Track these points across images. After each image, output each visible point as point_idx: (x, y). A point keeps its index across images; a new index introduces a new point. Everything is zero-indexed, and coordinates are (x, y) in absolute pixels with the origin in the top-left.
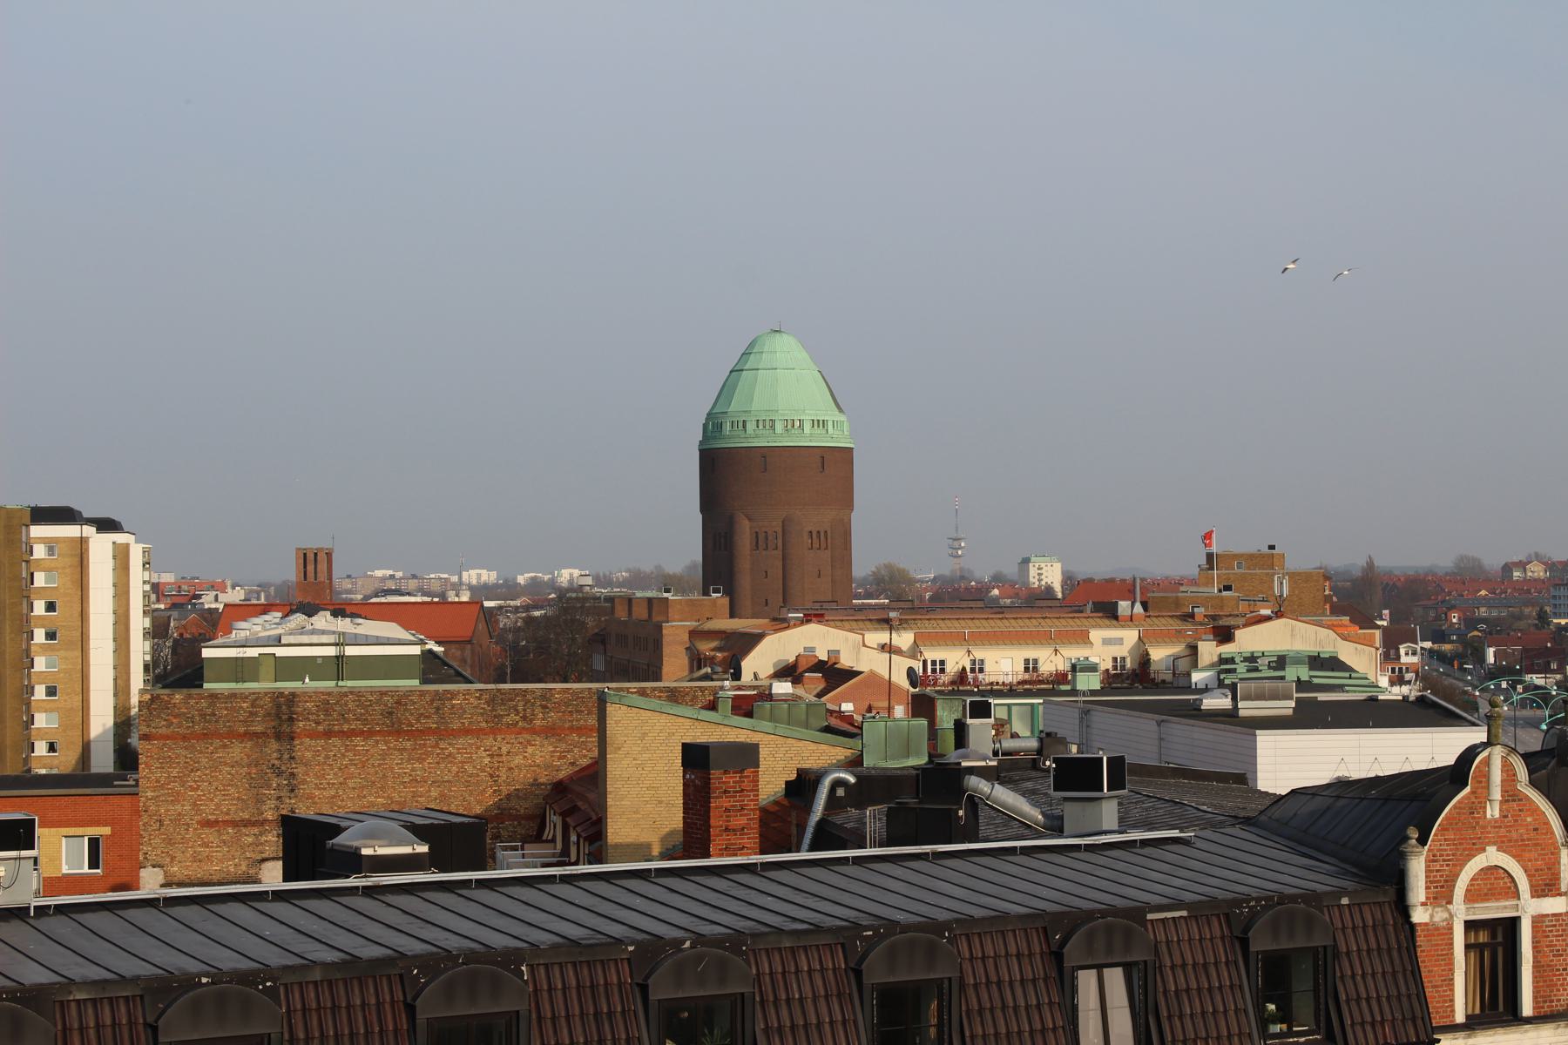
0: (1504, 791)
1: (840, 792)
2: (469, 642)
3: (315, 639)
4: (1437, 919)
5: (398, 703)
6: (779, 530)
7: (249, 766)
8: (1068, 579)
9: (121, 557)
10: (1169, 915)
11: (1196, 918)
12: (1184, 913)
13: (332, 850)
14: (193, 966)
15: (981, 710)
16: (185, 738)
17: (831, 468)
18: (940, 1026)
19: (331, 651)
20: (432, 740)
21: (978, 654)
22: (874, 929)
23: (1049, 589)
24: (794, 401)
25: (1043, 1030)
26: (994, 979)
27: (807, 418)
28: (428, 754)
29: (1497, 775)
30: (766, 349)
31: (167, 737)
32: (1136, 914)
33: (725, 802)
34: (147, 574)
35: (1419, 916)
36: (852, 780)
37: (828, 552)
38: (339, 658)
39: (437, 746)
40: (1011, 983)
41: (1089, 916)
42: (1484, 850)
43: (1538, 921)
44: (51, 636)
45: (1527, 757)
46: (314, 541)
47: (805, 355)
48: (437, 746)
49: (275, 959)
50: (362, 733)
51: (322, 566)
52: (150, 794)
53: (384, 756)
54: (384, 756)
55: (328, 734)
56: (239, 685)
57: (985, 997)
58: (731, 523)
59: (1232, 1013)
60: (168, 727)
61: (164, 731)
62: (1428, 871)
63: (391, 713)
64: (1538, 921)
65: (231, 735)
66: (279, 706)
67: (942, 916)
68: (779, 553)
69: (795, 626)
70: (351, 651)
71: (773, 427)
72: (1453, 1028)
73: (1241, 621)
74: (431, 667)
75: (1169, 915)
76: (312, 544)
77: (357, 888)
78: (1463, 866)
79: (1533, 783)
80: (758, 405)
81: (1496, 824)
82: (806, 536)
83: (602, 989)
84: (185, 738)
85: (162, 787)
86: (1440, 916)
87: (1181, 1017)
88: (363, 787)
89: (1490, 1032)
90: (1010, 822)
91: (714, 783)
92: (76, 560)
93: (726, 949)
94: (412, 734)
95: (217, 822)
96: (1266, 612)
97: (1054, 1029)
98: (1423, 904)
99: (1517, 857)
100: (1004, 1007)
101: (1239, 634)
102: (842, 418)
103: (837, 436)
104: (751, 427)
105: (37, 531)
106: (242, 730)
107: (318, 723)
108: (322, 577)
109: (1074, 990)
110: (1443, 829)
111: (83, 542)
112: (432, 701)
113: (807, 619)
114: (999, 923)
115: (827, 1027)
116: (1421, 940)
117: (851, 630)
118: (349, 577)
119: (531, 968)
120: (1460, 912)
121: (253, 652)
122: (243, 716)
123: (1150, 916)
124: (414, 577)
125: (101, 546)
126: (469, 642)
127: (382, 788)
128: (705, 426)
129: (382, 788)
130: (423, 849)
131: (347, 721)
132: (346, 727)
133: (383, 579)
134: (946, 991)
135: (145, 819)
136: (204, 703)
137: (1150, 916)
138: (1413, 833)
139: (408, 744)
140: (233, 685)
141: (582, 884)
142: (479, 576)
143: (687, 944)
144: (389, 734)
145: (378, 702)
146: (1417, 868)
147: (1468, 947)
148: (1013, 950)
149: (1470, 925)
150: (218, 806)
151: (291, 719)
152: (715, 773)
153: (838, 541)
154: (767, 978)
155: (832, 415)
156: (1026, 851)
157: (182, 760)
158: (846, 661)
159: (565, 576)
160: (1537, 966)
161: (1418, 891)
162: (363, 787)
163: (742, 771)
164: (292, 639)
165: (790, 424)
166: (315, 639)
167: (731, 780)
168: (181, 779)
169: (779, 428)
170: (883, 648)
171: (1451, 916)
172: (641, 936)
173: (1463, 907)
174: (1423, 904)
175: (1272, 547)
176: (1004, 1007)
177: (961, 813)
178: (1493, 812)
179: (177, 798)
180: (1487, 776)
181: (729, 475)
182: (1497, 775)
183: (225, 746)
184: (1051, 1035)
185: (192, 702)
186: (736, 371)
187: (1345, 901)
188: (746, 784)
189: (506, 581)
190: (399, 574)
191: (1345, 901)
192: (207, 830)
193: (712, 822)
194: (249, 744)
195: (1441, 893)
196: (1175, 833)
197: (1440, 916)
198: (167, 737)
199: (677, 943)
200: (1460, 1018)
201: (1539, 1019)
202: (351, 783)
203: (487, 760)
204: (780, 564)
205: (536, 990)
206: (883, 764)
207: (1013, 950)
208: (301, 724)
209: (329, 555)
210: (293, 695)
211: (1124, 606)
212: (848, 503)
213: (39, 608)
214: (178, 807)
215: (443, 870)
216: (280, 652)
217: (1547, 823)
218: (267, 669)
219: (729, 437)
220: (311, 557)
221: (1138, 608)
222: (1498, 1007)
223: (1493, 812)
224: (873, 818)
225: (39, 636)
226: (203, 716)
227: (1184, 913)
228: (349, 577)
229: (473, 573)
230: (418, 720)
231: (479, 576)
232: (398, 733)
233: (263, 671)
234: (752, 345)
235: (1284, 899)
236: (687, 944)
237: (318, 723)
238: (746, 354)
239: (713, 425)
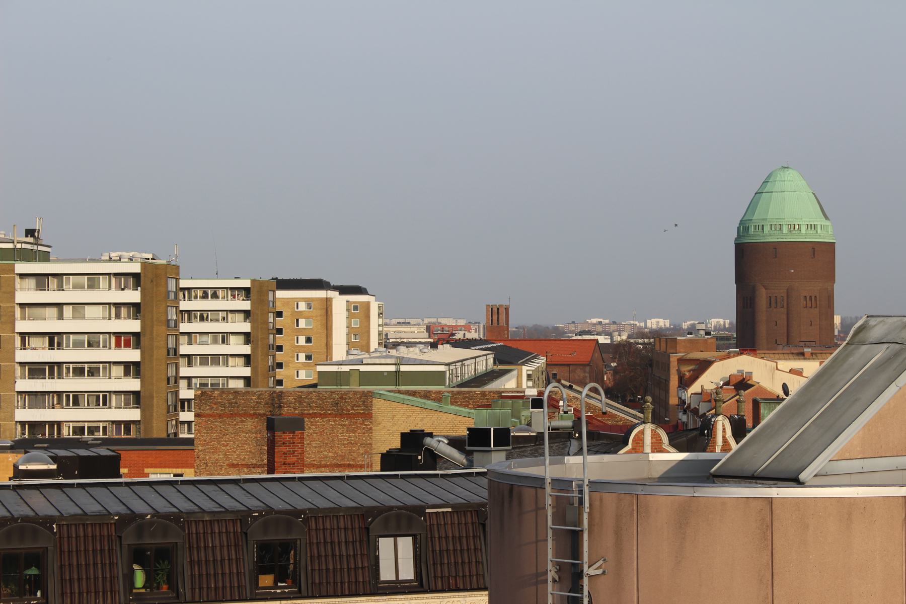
2: (588, 365)
5: (341, 398)
6: (785, 295)
7: (256, 433)
9: (360, 313)
10: (440, 510)
11: (457, 512)
12: (450, 510)
16: (220, 416)
17: (821, 255)
18: (295, 563)
19: (393, 368)
20: (360, 420)
22: (260, 512)
24: (795, 212)
25: (356, 568)
26: (329, 540)
28: (358, 428)
30: (778, 179)
31: (211, 416)
32: (419, 510)
33: (284, 449)
34: (381, 320)
37: (817, 310)
38: (397, 372)
39: (363, 423)
40: (339, 543)
44: (308, 357)
46: (497, 301)
47: (804, 182)
48: (363, 423)
50: (320, 415)
51: (503, 317)
52: (200, 448)
53: (333, 428)
54: (333, 428)
55: (232, 415)
57: (322, 549)
58: (754, 290)
59: (474, 563)
60: (211, 410)
61: (208, 412)
63: (337, 404)
65: (246, 415)
66: (273, 399)
68: (784, 310)
69: (734, 356)
70: (403, 368)
71: (781, 229)
75: (440, 510)
76: (497, 302)
80: (772, 214)
82: (802, 299)
83: (98, 538)
84: (220, 416)
85: (207, 444)
87: (441, 564)
88: (320, 447)
90: (450, 463)
91: (277, 439)
92: (324, 311)
93: (171, 520)
94: (348, 416)
95: (238, 465)
97: (363, 568)
100: (333, 555)
102: (828, 223)
103: (824, 235)
104: (767, 229)
105: (281, 294)
106: (252, 412)
107: (295, 409)
108: (503, 322)
109: (377, 548)
111: (328, 301)
112: (361, 397)
115: (227, 562)
117: (762, 358)
118: (573, 322)
119: (59, 526)
121: (346, 368)
122: (253, 404)
123: (427, 511)
124: (614, 323)
125: (340, 303)
126: (588, 365)
127: (332, 447)
128: (739, 228)
129: (332, 447)
130: (54, 467)
131: (312, 408)
132: (311, 411)
133: (594, 325)
134: (298, 546)
135: (198, 462)
136: (231, 396)
137: (427, 511)
139: (347, 422)
141: (442, 502)
142: (658, 322)
143: (149, 517)
144: (336, 416)
145: (330, 397)
148: (342, 525)
150: (239, 455)
151: (280, 406)
152: (278, 433)
153: (827, 305)
154: (194, 536)
155: (820, 221)
156: (403, 476)
157: (219, 429)
159: (654, 323)
162: (320, 447)
163: (294, 433)
164: (369, 361)
165: (792, 227)
167: (287, 437)
168: (218, 440)
169: (785, 229)
170: (792, 371)
176: (333, 555)
177: (420, 457)
179: (215, 451)
180: (642, 440)
181: (752, 259)
183: (242, 421)
184: (360, 571)
185: (224, 396)
186: (759, 193)
188: (296, 440)
189: (675, 326)
190: (607, 321)
192: (232, 469)
193: (276, 460)
194: (256, 420)
198: (211, 416)
199: (142, 516)
202: (314, 444)
204: (785, 317)
205: (60, 537)
207: (342, 525)
208: (286, 409)
209: (507, 309)
212: (831, 277)
213: (302, 340)
214: (216, 456)
215: (65, 478)
216: (363, 368)
218: (355, 379)
219: (753, 236)
220: (495, 310)
225: (302, 357)
226: (230, 403)
227: (450, 510)
228: (573, 322)
229: (654, 321)
230: (352, 408)
231: (658, 322)
232: (341, 415)
233: (352, 380)
234: (769, 176)
236: (149, 517)
237: (295, 409)
238: (765, 182)
239: (744, 227)
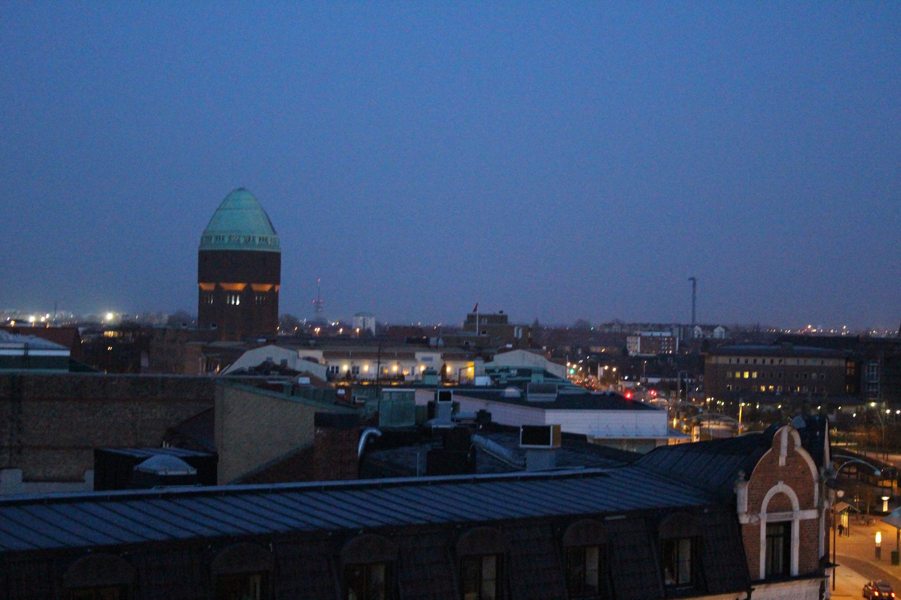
0: (788, 451)
1: (372, 441)
3: (9, 345)
4: (752, 521)
8: (378, 326)
12: (624, 517)
13: (138, 472)
14: (83, 543)
15: (445, 396)
19: (21, 353)
21: (357, 364)
23: (369, 330)
27: (257, 236)
29: (784, 442)
32: (599, 517)
35: (744, 520)
36: (379, 433)
41: (575, 517)
42: (777, 483)
43: (803, 523)
45: (799, 430)
49: (129, 538)
56: (26, 370)
62: (749, 494)
64: (803, 523)
67: (498, 517)
70: (32, 353)
72: (761, 582)
73: (495, 351)
74: (70, 363)
77: (158, 495)
78: (766, 492)
79: (803, 445)
81: (783, 469)
86: (754, 520)
89: (777, 585)
96: (509, 346)
98: (746, 513)
99: (794, 489)
101: (496, 357)
110: (757, 471)
113: (267, 343)
114: (528, 522)
116: (744, 533)
120: (764, 518)
138: (742, 474)
139: (86, 406)
140: (19, 370)
146: (743, 493)
147: (767, 536)
149: (769, 525)
158: (290, 365)
160: (801, 548)
161: (743, 506)
166: (9, 345)
171: (760, 520)
172: (335, 528)
173: (766, 515)
174: (746, 513)
175: (501, 312)
178: (782, 461)
181: (216, 264)
182: (784, 442)
187: (706, 511)
191: (706, 511)
195: (754, 508)
196: (598, 470)
197: (754, 520)
200: (762, 575)
201: (802, 577)
203: (130, 416)
206: (396, 426)
210: (22, 377)
211: (433, 341)
217: (808, 468)
221: (441, 342)
222: (780, 573)
223: (782, 461)
224: (418, 456)
227: (624, 517)
235: (675, 509)
236: (361, 532)
